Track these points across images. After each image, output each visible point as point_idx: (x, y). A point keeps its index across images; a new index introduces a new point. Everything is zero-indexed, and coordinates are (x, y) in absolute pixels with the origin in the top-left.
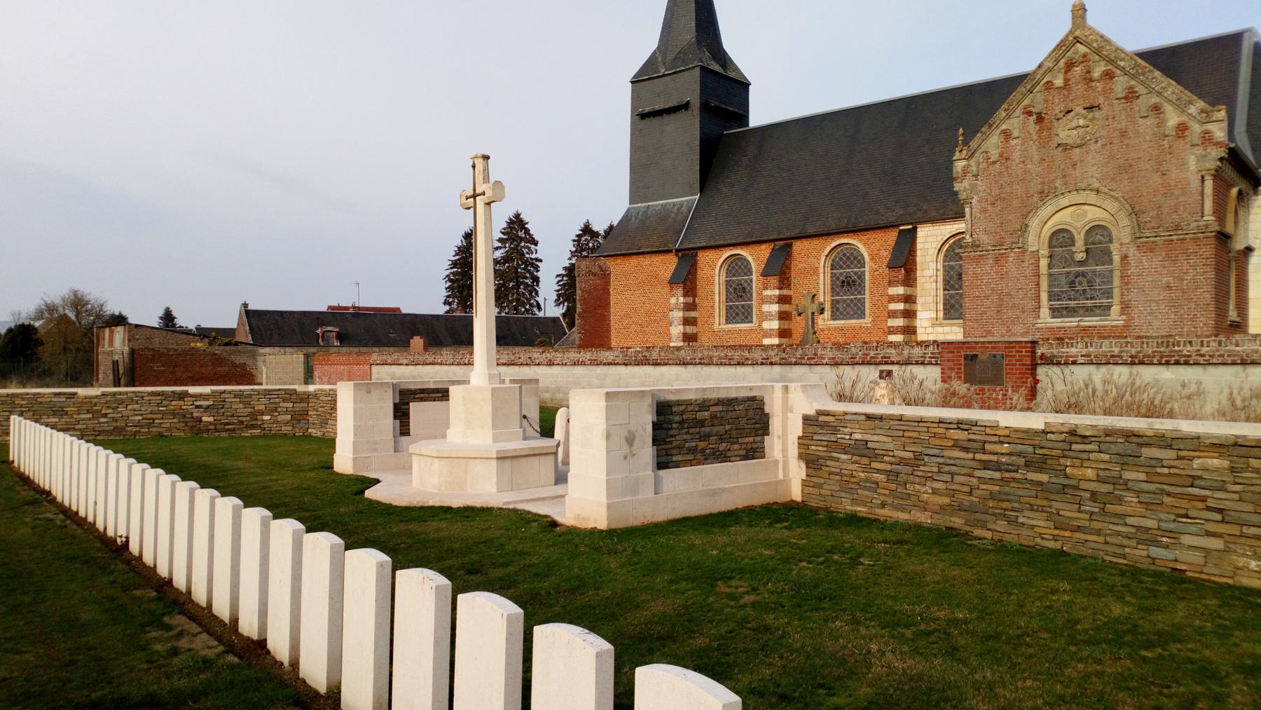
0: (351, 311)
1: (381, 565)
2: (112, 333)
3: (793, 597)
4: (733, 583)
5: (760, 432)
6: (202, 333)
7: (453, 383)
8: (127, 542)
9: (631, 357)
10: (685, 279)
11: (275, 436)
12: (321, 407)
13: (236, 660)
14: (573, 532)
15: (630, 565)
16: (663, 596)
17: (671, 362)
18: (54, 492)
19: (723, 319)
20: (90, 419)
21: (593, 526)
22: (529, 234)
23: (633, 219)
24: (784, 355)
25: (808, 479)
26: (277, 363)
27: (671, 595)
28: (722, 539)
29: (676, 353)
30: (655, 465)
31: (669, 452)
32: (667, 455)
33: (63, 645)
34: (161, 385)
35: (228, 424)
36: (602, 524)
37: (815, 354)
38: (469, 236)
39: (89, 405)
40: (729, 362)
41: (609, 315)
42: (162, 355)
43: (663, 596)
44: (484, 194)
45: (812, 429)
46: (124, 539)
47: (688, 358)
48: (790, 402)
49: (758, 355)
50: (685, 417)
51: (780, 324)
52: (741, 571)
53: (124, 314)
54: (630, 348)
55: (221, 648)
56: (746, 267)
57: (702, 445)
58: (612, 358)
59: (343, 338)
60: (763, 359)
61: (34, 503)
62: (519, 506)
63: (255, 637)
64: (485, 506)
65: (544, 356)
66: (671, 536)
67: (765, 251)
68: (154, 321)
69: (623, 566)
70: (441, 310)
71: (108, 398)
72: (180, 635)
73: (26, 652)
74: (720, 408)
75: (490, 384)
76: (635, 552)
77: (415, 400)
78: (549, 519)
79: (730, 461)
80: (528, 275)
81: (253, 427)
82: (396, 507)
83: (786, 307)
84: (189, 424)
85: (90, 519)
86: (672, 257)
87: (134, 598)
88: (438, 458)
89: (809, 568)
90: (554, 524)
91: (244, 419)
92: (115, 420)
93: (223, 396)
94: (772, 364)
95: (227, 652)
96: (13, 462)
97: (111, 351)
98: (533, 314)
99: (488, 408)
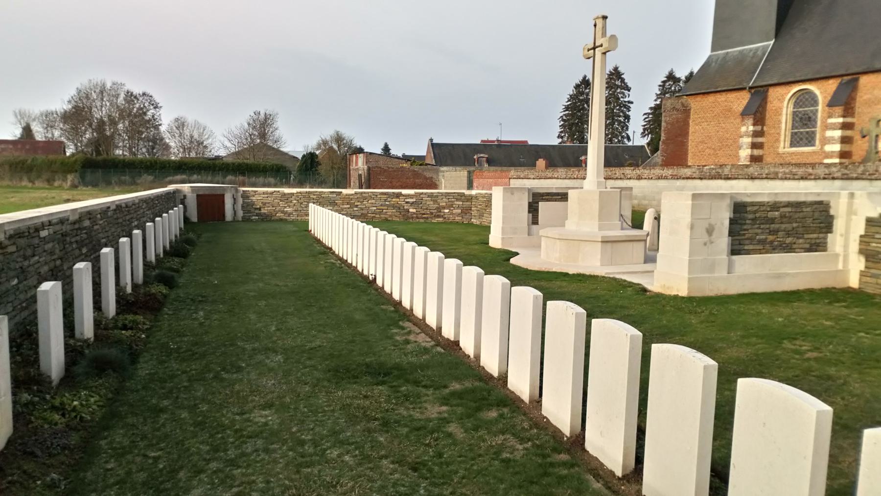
0: (496, 143)
1: (536, 297)
2: (357, 158)
3: (853, 357)
4: (798, 342)
5: (824, 230)
6: (406, 158)
7: (570, 188)
8: (375, 278)
9: (706, 173)
10: (756, 111)
11: (451, 223)
12: (480, 205)
13: (442, 350)
14: (659, 296)
15: (708, 322)
16: (737, 346)
17: (740, 177)
18: (333, 249)
19: (788, 144)
20: (349, 208)
21: (676, 293)
22: (624, 83)
23: (714, 64)
24: (846, 171)
25: (867, 270)
26: (451, 177)
27: (744, 346)
28: (787, 311)
29: (746, 170)
30: (730, 251)
31: (742, 242)
32: (740, 244)
33: (347, 331)
34: (385, 188)
35: (424, 214)
36: (683, 292)
37: (877, 171)
38: (586, 83)
39: (348, 199)
40: (793, 177)
41: (687, 142)
42: (385, 171)
43: (737, 346)
44: (601, 46)
45: (874, 229)
46: (374, 277)
47: (756, 173)
48: (855, 207)
49: (821, 171)
50: (757, 215)
51: (841, 147)
52: (805, 335)
53: (362, 147)
54: (705, 166)
55: (433, 343)
56: (813, 99)
57: (771, 238)
58: (690, 173)
59: (490, 162)
60: (825, 174)
61: (324, 253)
62: (618, 276)
63: (452, 339)
64: (592, 274)
65: (634, 172)
66: (742, 305)
67: (832, 85)
68: (379, 151)
69: (702, 322)
70: (556, 142)
71: (358, 196)
72: (410, 333)
73: (329, 333)
74: (789, 209)
75: (598, 188)
76: (711, 314)
77: (543, 200)
78: (641, 286)
79: (794, 252)
80: (621, 114)
81: (439, 216)
82: (531, 270)
83: (849, 133)
84: (402, 213)
85: (354, 264)
86: (745, 94)
87: (382, 310)
88: (559, 239)
89: (867, 338)
90: (645, 290)
91: (433, 211)
92: (362, 209)
93: (421, 196)
94: (833, 178)
95: (437, 345)
96: (311, 231)
97: (358, 168)
98: (623, 143)
99: (596, 206)
